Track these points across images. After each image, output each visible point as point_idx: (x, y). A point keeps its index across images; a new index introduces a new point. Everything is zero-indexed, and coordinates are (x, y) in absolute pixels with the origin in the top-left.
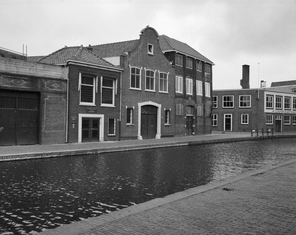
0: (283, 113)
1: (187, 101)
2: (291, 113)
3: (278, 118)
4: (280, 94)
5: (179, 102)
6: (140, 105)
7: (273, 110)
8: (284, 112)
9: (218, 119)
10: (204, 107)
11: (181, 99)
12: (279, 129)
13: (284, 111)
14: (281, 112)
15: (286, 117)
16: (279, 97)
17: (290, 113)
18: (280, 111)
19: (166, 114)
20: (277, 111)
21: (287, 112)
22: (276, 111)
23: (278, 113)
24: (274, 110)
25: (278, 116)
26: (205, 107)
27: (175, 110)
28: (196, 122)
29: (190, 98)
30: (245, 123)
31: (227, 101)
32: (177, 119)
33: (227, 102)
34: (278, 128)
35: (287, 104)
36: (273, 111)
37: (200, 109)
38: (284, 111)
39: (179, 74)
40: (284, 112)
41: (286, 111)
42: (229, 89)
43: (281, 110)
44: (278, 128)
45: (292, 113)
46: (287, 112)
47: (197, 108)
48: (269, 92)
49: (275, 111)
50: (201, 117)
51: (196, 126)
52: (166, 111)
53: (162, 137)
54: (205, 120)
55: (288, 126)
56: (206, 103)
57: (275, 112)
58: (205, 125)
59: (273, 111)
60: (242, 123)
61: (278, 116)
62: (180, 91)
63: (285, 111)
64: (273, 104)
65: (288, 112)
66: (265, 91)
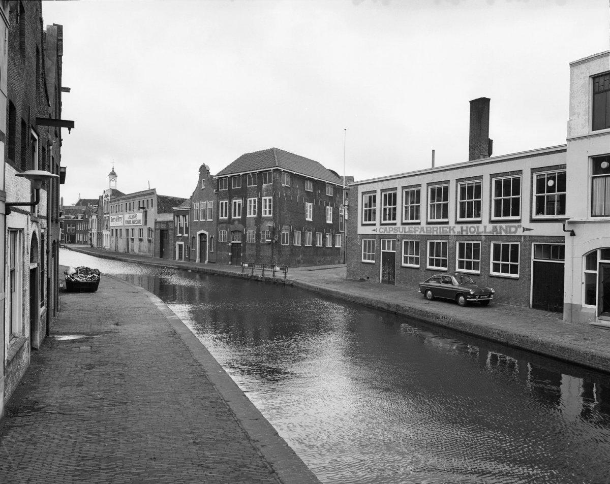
0: (398, 233)
1: (232, 226)
2: (420, 232)
3: (389, 248)
4: (390, 185)
5: (222, 228)
6: (198, 233)
7: (373, 228)
8: (401, 230)
9: (481, 259)
10: (258, 230)
11: (224, 225)
12: (389, 278)
13: (399, 228)
14: (392, 233)
15: (415, 245)
16: (390, 192)
17: (417, 233)
18: (389, 228)
19: (193, 240)
20: (383, 228)
21: (407, 230)
22: (382, 230)
23: (386, 233)
24: (377, 228)
25: (389, 242)
26: (260, 231)
27: (218, 237)
28: (244, 250)
29: (236, 223)
30: (500, 274)
31: (502, 197)
32: (219, 246)
33: (504, 200)
34: (389, 274)
35: (370, 210)
36: (374, 230)
37: (251, 233)
38: (399, 228)
39: (223, 199)
40: (401, 230)
41: (405, 228)
42: (405, 172)
43: (393, 227)
44: (389, 274)
45: (422, 233)
46: (407, 230)
47: (246, 233)
48: (367, 185)
49: (378, 230)
50: (252, 244)
51: (244, 255)
52: (212, 238)
53: (209, 262)
54: (259, 248)
55: (413, 270)
56: (262, 226)
57: (378, 233)
58: (259, 255)
59: (374, 230)
60: (492, 273)
61: (389, 242)
62: (331, 194)
63: (403, 228)
64: (381, 214)
65: (409, 231)
66: (359, 186)
